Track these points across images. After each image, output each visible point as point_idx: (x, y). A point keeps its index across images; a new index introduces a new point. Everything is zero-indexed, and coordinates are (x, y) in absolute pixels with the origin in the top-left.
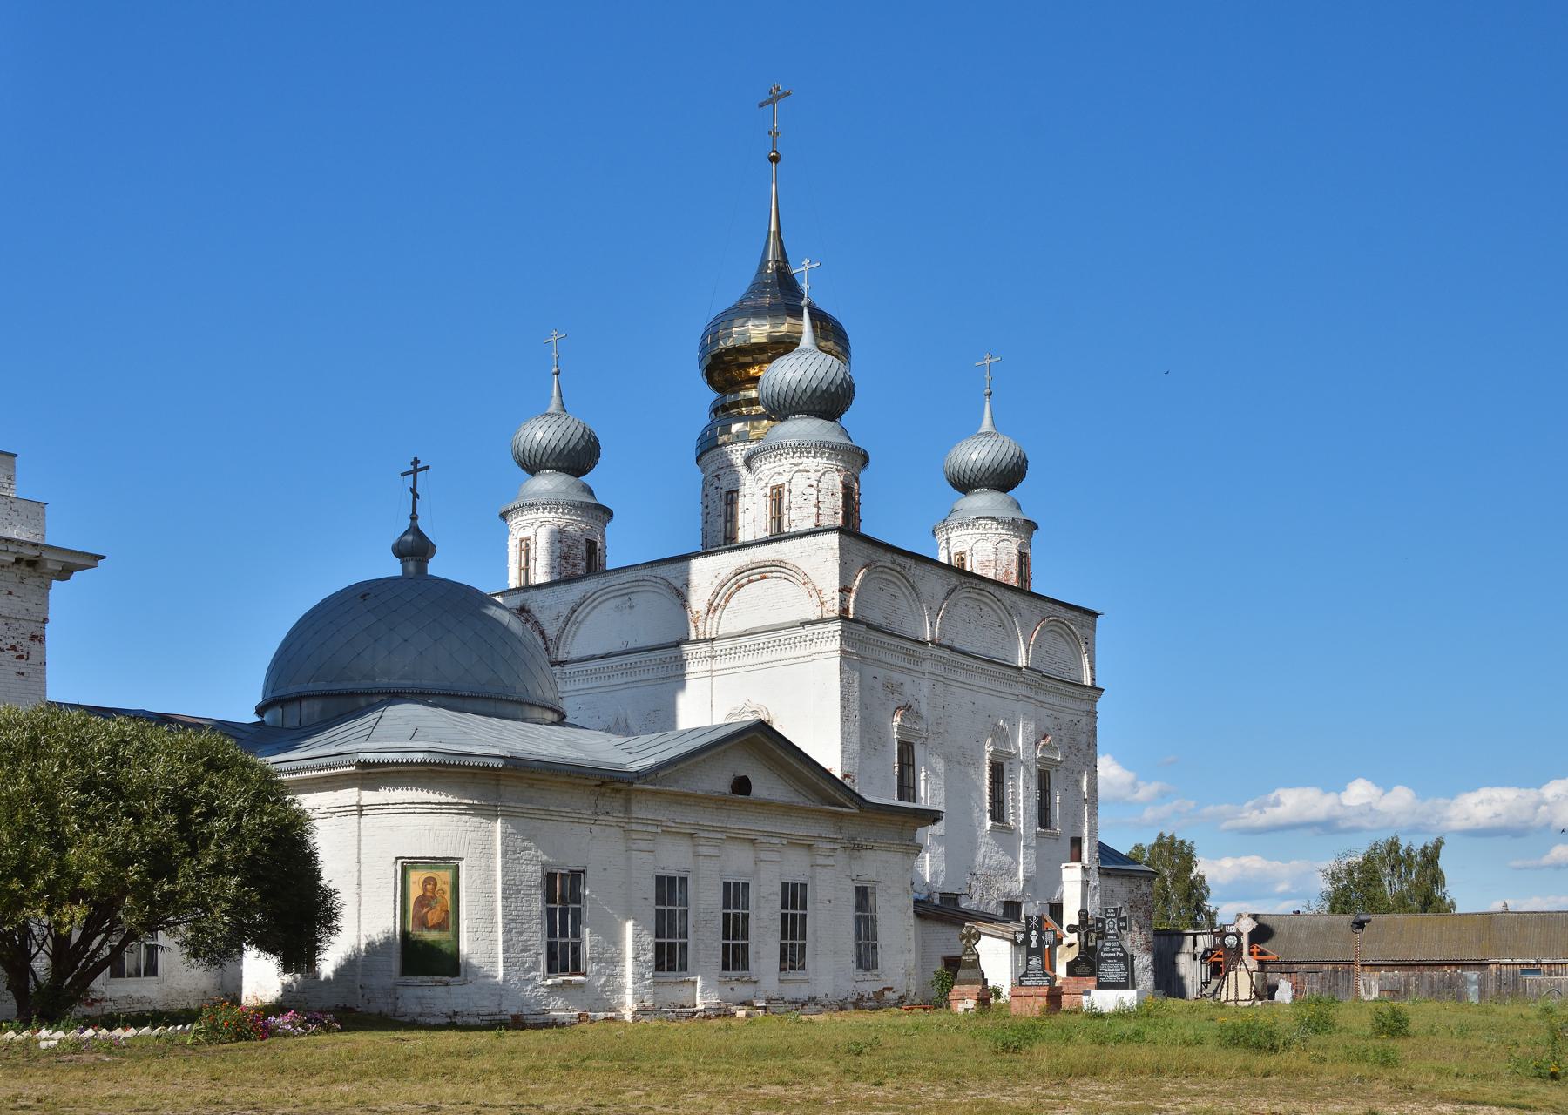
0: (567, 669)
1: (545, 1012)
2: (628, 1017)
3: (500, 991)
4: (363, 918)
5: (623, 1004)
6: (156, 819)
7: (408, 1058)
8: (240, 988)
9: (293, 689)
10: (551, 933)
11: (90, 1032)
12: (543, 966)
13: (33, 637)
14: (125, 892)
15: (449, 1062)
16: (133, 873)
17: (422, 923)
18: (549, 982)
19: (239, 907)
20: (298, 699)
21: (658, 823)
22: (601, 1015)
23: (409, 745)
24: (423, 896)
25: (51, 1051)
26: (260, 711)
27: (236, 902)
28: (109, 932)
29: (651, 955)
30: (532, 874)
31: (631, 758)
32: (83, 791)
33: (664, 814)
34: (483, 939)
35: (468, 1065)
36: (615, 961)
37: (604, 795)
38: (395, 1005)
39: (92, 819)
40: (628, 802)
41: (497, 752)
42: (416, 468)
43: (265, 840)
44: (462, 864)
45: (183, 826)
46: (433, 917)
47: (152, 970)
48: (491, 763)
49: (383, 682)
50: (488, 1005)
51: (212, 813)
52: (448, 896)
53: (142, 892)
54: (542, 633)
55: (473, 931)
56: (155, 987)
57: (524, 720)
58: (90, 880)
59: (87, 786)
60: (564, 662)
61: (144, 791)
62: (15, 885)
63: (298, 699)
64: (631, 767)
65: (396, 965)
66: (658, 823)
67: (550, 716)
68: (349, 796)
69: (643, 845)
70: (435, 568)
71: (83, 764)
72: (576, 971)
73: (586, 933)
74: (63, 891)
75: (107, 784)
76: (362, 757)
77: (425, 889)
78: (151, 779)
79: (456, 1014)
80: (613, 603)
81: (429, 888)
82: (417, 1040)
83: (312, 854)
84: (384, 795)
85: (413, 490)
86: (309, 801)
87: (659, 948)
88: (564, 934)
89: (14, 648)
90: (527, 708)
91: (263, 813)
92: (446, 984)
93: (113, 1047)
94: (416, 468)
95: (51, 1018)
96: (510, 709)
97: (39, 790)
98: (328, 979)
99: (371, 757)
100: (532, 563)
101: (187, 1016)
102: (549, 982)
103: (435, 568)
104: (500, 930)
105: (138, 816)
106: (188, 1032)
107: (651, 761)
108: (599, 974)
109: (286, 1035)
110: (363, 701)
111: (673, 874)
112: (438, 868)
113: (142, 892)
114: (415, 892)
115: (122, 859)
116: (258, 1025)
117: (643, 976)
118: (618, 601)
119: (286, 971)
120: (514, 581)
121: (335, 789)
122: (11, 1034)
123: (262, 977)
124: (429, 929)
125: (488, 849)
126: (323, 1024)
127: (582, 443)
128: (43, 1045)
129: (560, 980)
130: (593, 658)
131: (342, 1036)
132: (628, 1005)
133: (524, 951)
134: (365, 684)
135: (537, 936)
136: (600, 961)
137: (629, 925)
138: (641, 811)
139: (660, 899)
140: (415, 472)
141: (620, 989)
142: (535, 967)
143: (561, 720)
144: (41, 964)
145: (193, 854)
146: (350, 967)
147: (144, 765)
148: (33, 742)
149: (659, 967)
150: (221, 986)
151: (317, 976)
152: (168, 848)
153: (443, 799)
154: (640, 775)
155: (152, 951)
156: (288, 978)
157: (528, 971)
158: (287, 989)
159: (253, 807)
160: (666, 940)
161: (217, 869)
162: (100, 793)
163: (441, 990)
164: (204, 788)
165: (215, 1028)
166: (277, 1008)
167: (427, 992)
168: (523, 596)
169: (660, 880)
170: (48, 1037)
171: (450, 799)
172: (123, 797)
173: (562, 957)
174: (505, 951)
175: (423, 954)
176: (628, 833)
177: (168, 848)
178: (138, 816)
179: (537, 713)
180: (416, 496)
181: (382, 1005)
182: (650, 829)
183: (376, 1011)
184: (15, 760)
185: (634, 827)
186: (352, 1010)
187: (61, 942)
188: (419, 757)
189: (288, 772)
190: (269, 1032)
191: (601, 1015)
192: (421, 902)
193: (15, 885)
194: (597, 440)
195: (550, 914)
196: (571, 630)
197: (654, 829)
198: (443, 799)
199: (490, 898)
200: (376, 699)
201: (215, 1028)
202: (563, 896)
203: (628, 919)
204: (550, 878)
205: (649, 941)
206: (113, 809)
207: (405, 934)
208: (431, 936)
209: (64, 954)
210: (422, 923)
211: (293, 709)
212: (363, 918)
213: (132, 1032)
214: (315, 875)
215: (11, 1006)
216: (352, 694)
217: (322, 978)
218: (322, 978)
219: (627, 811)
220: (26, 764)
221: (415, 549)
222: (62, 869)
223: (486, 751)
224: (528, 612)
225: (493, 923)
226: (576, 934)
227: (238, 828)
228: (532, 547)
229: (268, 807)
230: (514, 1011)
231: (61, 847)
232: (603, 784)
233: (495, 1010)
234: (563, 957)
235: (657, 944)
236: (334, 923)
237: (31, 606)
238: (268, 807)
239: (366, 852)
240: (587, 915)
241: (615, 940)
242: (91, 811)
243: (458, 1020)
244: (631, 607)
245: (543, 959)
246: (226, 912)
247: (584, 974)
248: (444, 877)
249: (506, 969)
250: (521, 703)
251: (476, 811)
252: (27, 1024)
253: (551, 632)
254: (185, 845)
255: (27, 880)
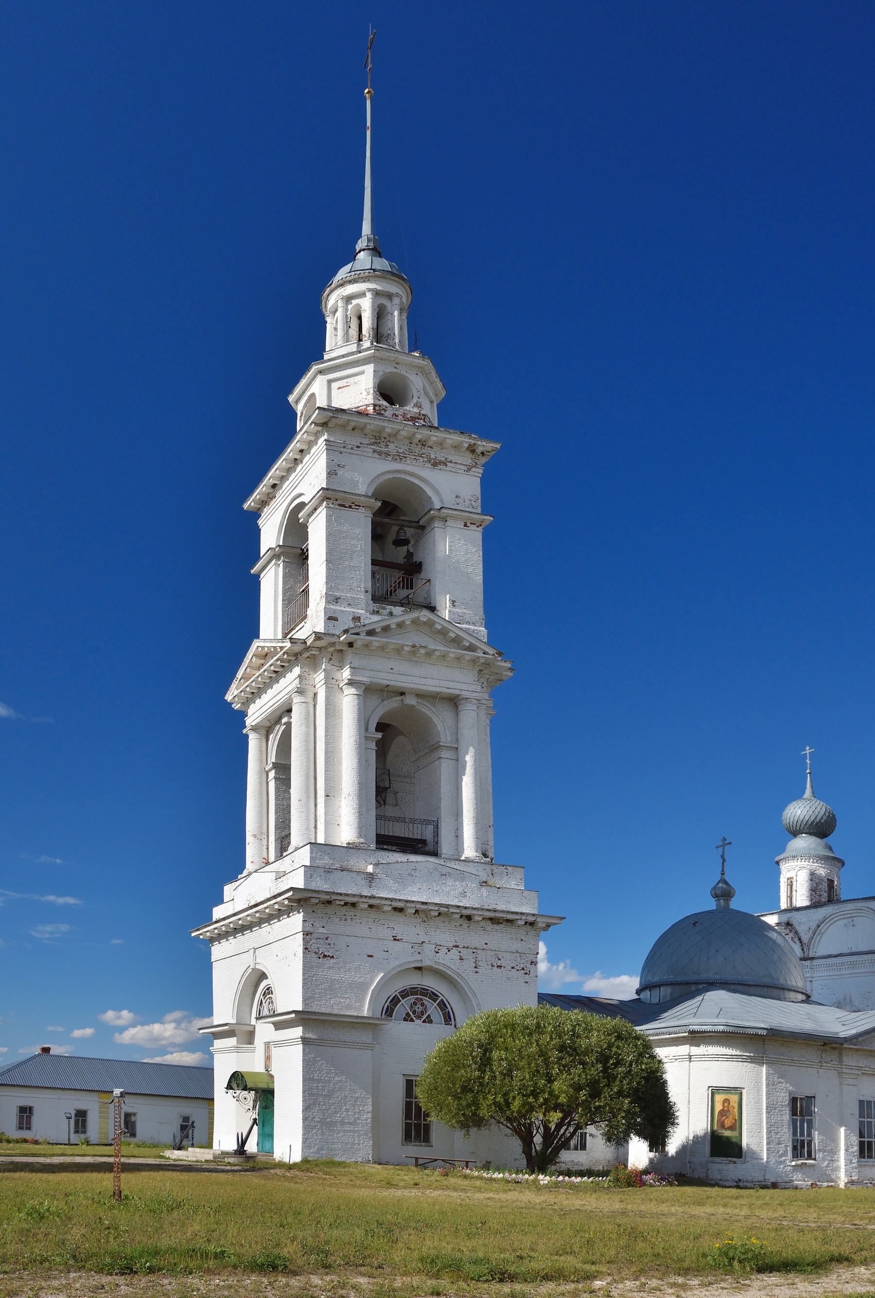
0: (815, 962)
1: (791, 1181)
2: (842, 1185)
3: (765, 1168)
4: (690, 1123)
5: (839, 1178)
6: (593, 1066)
7: (708, 1198)
8: (627, 1160)
9: (656, 979)
10: (795, 1133)
11: (561, 1178)
12: (790, 1154)
13: (532, 962)
14: (578, 1105)
15: (726, 1200)
16: (583, 1095)
17: (722, 1125)
18: (793, 1163)
19: (630, 1115)
20: (658, 986)
21: (860, 1068)
22: (826, 1184)
23: (716, 1021)
24: (723, 1110)
25: (546, 1186)
26: (638, 992)
27: (628, 1112)
28: (569, 1124)
29: (856, 1148)
30: (784, 1098)
31: (844, 1028)
32: (560, 1051)
33: (863, 1062)
34: (755, 1135)
35: (734, 1202)
36: (833, 1152)
37: (826, 1051)
38: (707, 1173)
39: (564, 1066)
40: (841, 1054)
41: (763, 1026)
42: (725, 843)
43: (644, 1078)
44: (744, 1092)
45: (605, 1070)
46: (728, 1122)
47: (583, 1147)
48: (760, 1032)
49: (704, 976)
50: (758, 1176)
51: (618, 1063)
52: (736, 1110)
53: (586, 1105)
54: (800, 939)
55: (750, 1131)
56: (585, 1157)
57: (785, 1000)
58: (563, 1099)
59: (562, 1048)
60: (812, 958)
61: (586, 1053)
62: (531, 1100)
63: (658, 986)
64: (842, 1035)
65: (707, 1149)
66: (860, 1068)
67: (801, 997)
68: (684, 1049)
69: (850, 1081)
70: (735, 904)
71: (560, 1037)
72: (810, 1157)
73: (816, 1135)
74: (552, 1105)
75: (570, 1047)
76: (692, 1028)
77: (724, 1106)
78: (590, 1045)
79: (740, 1180)
80: (842, 922)
81: (726, 1104)
82: (715, 1191)
83: (665, 1082)
84: (702, 1050)
85: (722, 857)
86: (661, 1052)
87: (861, 1144)
88: (802, 1134)
89: (523, 969)
90: (786, 992)
91: (642, 1063)
92: (735, 1163)
93: (573, 1186)
94: (725, 843)
95: (543, 1170)
96: (776, 992)
97: (541, 1050)
98: (672, 1156)
99: (696, 1028)
100: (794, 893)
101: (605, 1173)
102: (793, 1163)
103: (735, 904)
104: (765, 1131)
105: (583, 1063)
106: (605, 1181)
107: (854, 1032)
108: (824, 1159)
109: (651, 1186)
110: (693, 988)
111: (870, 1099)
112: (730, 1093)
113: (586, 1105)
114: (718, 1107)
115: (578, 1088)
116: (636, 1180)
117: (851, 1161)
118: (845, 921)
119: (651, 1151)
120: (783, 905)
121: (677, 1045)
122: (527, 1176)
123: (639, 1153)
124: (726, 1129)
125: (758, 1082)
126: (669, 1181)
127: (825, 818)
128: (542, 1182)
129: (800, 1162)
130: (830, 956)
131: (678, 1188)
132: (842, 1179)
133: (779, 1144)
134: (695, 978)
135: (786, 1136)
136: (825, 1151)
137: (842, 1130)
138: (850, 1060)
139: (861, 1115)
140: (723, 846)
141: (837, 1169)
142: (785, 1154)
143: (808, 999)
144: (538, 1139)
145: (608, 1086)
146: (684, 1150)
147: (587, 1037)
148: (538, 1025)
149: (862, 1154)
150: (617, 1159)
151: (666, 1154)
152: (597, 1082)
153: (734, 1052)
154: (846, 1040)
155: (583, 1136)
156: (652, 1155)
157: (781, 1156)
158: (651, 1161)
159: (637, 1060)
160: (866, 1140)
161: (620, 1093)
162: (567, 1053)
163: (732, 1166)
164: (614, 1049)
165: (618, 1180)
166: (646, 1172)
167: (724, 1167)
168: (788, 915)
169: (861, 1103)
170: (544, 1179)
171: (738, 1053)
172: (578, 1054)
173: (801, 1148)
174: (768, 1144)
175: (722, 1145)
176: (840, 1074)
177: (597, 1082)
178: (583, 1063)
179: (792, 995)
180: (724, 860)
181: (699, 1173)
182: (854, 1072)
183: (697, 1177)
184: (530, 1034)
185: (845, 1071)
186: (684, 1175)
187: (547, 1128)
188: (721, 1028)
189: (654, 1035)
190: (643, 1184)
191: (826, 1184)
192: (722, 1113)
193: (531, 1100)
194: (834, 816)
195: (794, 1123)
196: (817, 938)
197: (857, 1072)
198: (734, 1052)
199: (760, 1113)
200: (701, 986)
201: (618, 1180)
202: (801, 1109)
203: (841, 1126)
204: (794, 1100)
205: (855, 1140)
206: (573, 1061)
207: (713, 1132)
208: (727, 1133)
209: (548, 1136)
210: (722, 1125)
211: (656, 992)
212: (690, 1123)
213: (579, 1179)
214: (665, 1095)
215: (524, 1162)
216: (687, 983)
217: (670, 1155)
218: (670, 1155)
219: (840, 1061)
220: (535, 1037)
221: (724, 893)
222: (551, 1093)
223: (757, 1025)
224: (791, 925)
225: (761, 1127)
226: (809, 1135)
227: (630, 1071)
228: (794, 883)
229: (645, 1060)
230: (773, 1180)
231: (550, 1081)
232: (825, 1044)
233: (762, 1179)
234: (801, 1148)
235: (860, 1142)
236: (676, 1121)
237: (531, 947)
238: (645, 1060)
239: (695, 1080)
240: (816, 1122)
241: (835, 1140)
242: (564, 1062)
243: (741, 1184)
244: (854, 926)
245: (790, 1149)
246: (623, 1118)
247: (815, 1159)
248: (734, 1098)
249: (768, 1154)
250: (784, 989)
251: (752, 1060)
252: (532, 1172)
253: (805, 938)
254: (605, 1080)
255: (536, 1097)
